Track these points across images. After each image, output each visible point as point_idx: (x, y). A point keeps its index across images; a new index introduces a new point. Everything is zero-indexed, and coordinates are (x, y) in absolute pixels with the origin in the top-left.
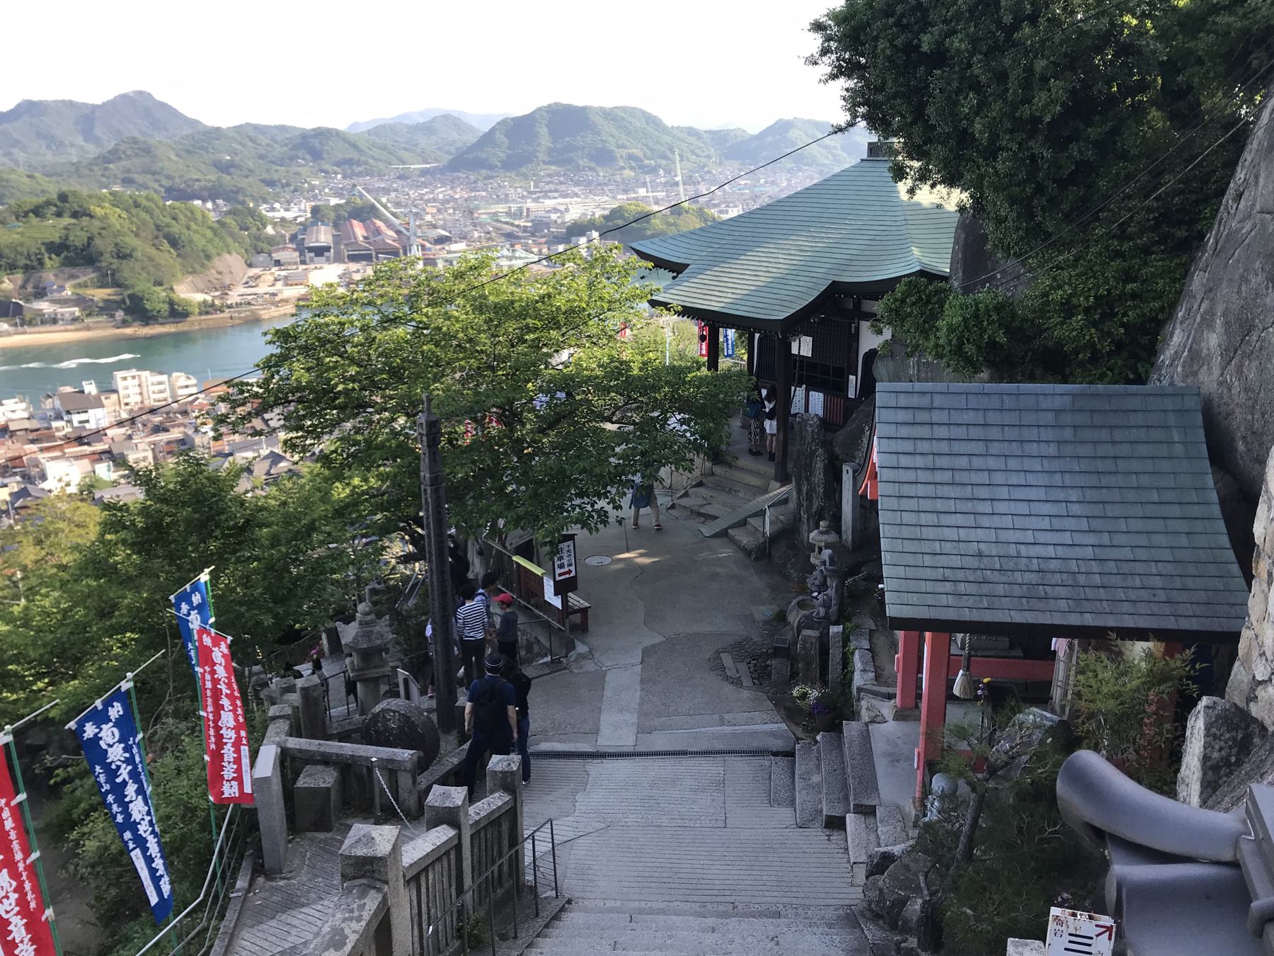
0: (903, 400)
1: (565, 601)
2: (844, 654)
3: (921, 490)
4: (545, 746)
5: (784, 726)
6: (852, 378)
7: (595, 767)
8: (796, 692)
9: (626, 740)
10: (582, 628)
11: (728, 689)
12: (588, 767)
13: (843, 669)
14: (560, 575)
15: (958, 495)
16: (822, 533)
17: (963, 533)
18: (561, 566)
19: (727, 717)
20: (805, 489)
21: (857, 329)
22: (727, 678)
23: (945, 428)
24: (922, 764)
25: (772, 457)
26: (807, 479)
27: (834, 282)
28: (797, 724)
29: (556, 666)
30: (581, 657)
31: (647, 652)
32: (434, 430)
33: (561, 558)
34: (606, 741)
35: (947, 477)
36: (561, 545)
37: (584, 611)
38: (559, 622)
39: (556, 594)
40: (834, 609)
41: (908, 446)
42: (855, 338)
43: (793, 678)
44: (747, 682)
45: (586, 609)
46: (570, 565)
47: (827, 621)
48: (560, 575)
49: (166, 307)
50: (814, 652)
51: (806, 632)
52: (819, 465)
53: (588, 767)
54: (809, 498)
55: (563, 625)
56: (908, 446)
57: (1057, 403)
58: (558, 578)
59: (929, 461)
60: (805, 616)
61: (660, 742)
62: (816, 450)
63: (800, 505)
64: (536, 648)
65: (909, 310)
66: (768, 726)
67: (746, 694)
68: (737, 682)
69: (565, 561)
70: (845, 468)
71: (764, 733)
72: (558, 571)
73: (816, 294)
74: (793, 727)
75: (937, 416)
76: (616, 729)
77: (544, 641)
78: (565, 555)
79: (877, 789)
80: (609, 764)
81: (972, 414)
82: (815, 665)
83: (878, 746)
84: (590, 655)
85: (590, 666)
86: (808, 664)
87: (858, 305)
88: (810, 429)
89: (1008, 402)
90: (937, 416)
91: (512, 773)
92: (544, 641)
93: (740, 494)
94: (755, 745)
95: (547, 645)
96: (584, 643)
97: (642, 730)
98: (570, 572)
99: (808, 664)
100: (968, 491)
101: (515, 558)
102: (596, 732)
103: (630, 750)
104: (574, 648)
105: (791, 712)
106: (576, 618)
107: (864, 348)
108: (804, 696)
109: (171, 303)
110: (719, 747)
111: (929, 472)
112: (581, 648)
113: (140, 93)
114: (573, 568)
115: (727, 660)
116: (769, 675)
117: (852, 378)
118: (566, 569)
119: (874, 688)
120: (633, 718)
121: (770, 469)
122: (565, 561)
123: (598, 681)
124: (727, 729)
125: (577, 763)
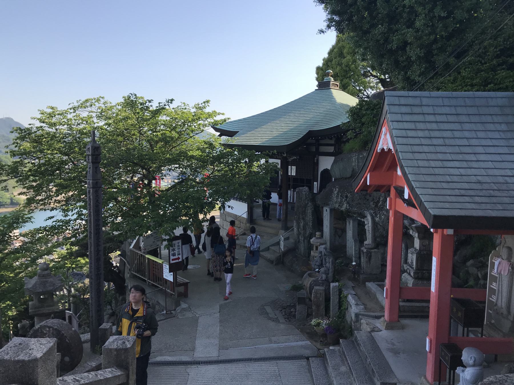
0: (403, 101)
1: (175, 278)
2: (340, 298)
3: (426, 149)
4: (159, 359)
5: (308, 342)
6: (315, 183)
7: (193, 370)
8: (313, 322)
9: (214, 354)
10: (184, 295)
11: (272, 324)
12: (188, 370)
13: (339, 308)
14: (173, 260)
15: (451, 151)
16: (317, 238)
17: (462, 171)
18: (174, 255)
19: (273, 339)
20: (302, 224)
21: (318, 160)
22: (270, 319)
23: (433, 116)
24: (433, 347)
25: (279, 220)
26: (303, 219)
27: (310, 131)
28: (316, 341)
29: (169, 315)
30: (184, 309)
31: (221, 306)
32: (97, 153)
33: (174, 250)
34: (200, 354)
35: (440, 141)
36: (174, 242)
37: (186, 285)
38: (171, 290)
39: (170, 272)
40: (331, 275)
41: (412, 126)
42: (317, 164)
43: (309, 316)
44: (282, 320)
45: (187, 283)
46: (179, 254)
47: (327, 282)
48: (173, 260)
49: (9, 201)
50: (322, 299)
51: (316, 288)
52: (309, 211)
53: (188, 370)
54: (304, 229)
55: (174, 292)
56: (412, 126)
57: (500, 102)
58: (172, 262)
59: (427, 134)
60: (314, 281)
61: (234, 354)
62: (308, 203)
63: (299, 234)
64: (157, 307)
65: (364, 112)
66: (300, 343)
67: (282, 326)
68: (276, 320)
69: (176, 252)
70: (325, 209)
71: (302, 347)
72: (172, 258)
73: (302, 136)
74: (314, 343)
75: (426, 110)
76: (205, 347)
77: (162, 303)
78: (176, 248)
79: (392, 371)
80: (203, 368)
81: (447, 108)
82: (322, 307)
83: (383, 346)
84: (189, 309)
85: (189, 315)
86: (318, 306)
87: (317, 149)
88: (304, 193)
89: (468, 102)
90: (426, 110)
91: (126, 350)
92: (162, 303)
93: (264, 237)
94: (293, 353)
95: (164, 305)
96: (185, 302)
97: (222, 348)
98: (179, 258)
99: (318, 306)
100: (457, 149)
101: (147, 256)
102: (193, 350)
103: (216, 359)
104: (180, 305)
105: (312, 335)
106: (182, 289)
107: (321, 168)
108: (318, 324)
109: (11, 199)
110: (272, 355)
111: (428, 139)
112: (184, 305)
113: (8, 118)
114: (180, 256)
115: (268, 309)
116: (294, 316)
117: (315, 183)
118: (176, 257)
119: (366, 313)
120: (216, 341)
121: (279, 225)
122: (176, 252)
123: (195, 321)
124: (275, 345)
125: (181, 368)
